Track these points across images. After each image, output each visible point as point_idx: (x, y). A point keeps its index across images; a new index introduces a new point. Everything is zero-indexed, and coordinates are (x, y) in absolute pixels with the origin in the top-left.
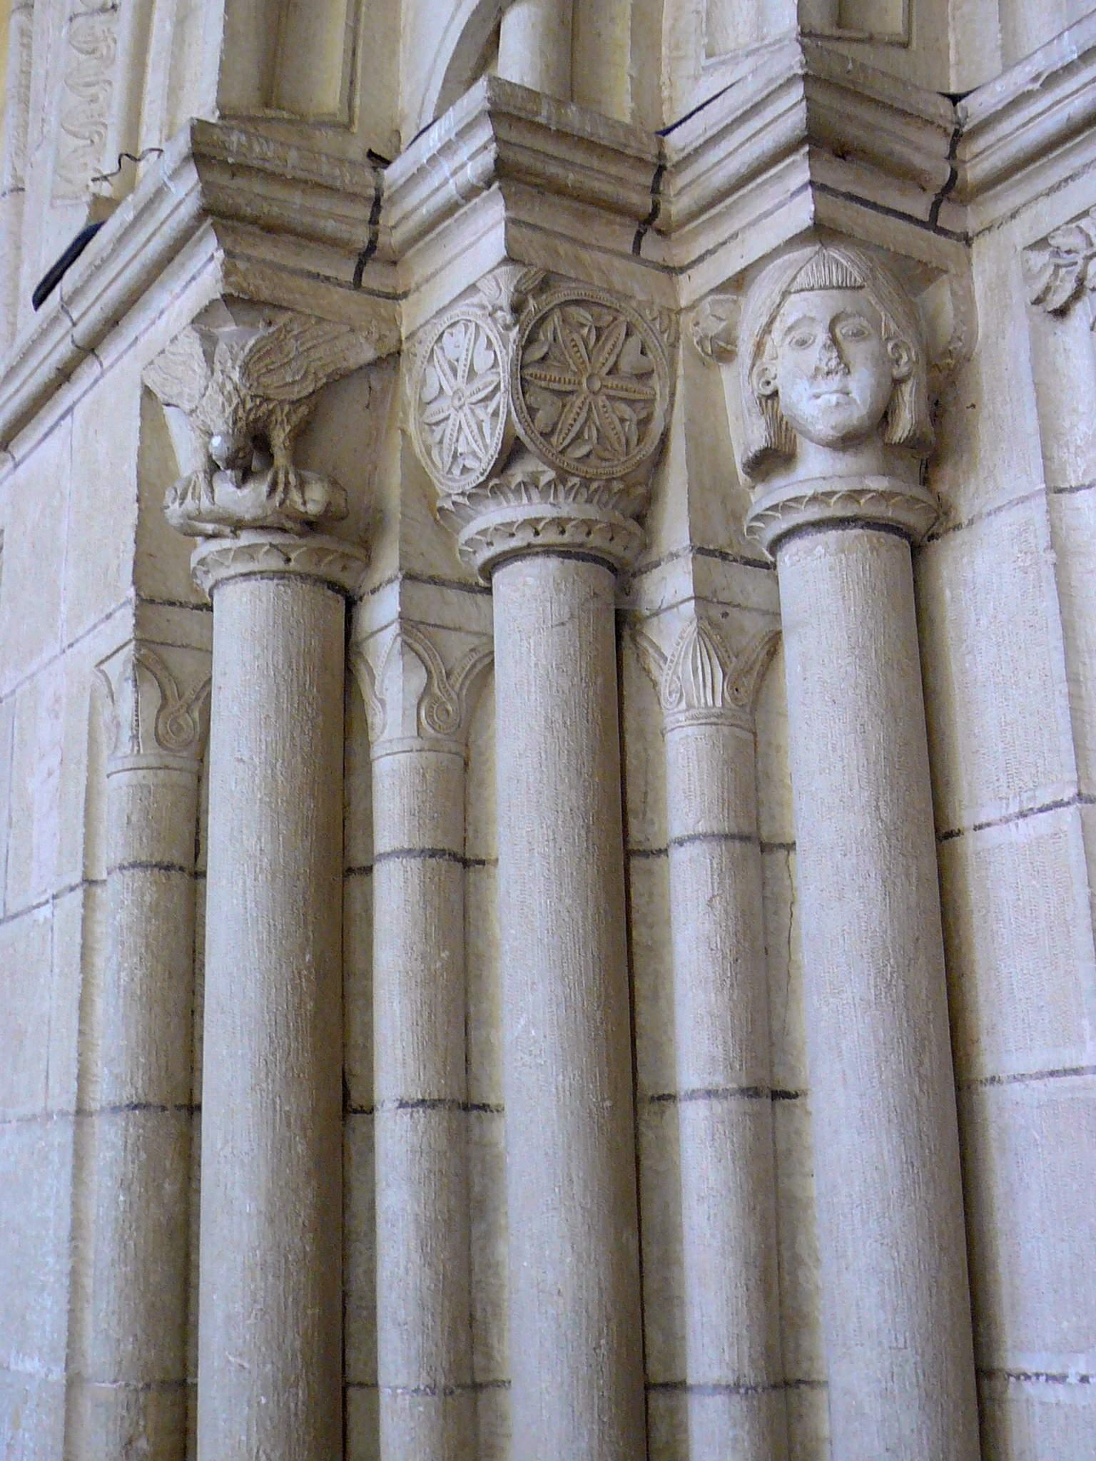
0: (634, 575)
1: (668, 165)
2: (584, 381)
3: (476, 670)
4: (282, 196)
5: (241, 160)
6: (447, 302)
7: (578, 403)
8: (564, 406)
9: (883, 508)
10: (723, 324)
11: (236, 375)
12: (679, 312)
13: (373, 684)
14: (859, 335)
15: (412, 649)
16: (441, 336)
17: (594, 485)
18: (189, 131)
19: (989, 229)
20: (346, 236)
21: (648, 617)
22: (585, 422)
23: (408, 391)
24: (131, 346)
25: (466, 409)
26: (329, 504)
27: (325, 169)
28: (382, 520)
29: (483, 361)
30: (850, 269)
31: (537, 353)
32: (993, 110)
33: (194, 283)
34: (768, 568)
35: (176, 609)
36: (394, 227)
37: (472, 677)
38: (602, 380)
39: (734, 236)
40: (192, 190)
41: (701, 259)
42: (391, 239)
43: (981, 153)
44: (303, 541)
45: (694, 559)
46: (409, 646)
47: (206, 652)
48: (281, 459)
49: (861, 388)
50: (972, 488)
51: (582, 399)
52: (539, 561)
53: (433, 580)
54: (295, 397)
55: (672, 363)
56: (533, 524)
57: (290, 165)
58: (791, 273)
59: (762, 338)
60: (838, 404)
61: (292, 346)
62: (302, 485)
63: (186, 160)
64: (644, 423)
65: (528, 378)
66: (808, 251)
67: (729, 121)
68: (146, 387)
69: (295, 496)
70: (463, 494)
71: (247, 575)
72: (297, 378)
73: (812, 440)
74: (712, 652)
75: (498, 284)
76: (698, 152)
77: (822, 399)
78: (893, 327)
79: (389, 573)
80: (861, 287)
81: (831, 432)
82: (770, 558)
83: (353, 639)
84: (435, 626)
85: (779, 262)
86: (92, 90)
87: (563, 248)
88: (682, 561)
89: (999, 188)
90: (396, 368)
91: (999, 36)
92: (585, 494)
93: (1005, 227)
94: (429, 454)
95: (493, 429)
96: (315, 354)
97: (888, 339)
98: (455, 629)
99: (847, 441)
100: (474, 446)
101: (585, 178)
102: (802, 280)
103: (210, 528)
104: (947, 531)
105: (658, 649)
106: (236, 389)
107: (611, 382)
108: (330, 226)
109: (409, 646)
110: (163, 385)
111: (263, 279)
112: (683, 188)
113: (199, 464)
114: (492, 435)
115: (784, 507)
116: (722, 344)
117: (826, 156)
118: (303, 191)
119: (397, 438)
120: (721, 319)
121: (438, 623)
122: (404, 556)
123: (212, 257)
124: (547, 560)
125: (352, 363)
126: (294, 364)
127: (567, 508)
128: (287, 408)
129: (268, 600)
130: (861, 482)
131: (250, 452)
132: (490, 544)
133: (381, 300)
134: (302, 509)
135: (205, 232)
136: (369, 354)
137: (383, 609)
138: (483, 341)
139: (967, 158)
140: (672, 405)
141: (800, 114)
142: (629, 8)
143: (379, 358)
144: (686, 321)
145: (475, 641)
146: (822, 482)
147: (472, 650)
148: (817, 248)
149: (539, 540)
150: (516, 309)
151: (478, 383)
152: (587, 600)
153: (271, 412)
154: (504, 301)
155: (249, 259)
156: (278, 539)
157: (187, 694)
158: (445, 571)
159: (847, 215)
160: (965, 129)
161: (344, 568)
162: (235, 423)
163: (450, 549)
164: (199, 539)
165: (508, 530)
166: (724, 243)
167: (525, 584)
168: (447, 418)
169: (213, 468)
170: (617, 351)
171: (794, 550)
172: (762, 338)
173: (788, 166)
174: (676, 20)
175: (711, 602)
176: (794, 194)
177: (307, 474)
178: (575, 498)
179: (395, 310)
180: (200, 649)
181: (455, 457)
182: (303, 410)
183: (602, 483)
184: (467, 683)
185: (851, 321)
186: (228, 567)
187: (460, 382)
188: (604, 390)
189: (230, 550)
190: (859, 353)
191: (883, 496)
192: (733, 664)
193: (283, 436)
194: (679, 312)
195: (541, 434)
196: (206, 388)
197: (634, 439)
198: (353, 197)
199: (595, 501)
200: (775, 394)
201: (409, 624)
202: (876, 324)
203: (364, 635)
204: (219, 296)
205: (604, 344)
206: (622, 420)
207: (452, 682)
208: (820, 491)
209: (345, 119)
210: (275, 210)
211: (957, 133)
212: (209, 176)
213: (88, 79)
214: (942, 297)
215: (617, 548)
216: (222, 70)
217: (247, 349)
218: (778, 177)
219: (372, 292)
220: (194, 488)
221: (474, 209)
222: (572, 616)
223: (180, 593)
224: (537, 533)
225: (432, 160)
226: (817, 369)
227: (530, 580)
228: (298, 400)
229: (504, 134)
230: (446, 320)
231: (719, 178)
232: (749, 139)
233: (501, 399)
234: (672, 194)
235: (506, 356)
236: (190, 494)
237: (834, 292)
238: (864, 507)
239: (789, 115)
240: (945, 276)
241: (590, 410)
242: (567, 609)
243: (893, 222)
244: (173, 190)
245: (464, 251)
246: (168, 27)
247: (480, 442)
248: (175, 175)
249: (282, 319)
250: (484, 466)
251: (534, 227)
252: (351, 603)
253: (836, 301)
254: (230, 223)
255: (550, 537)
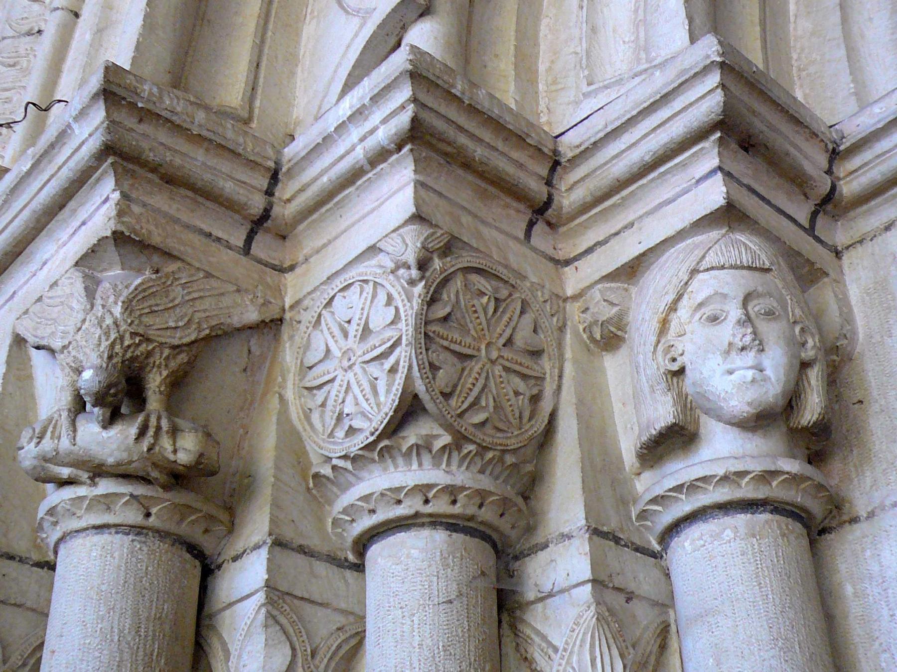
0: (516, 558)
1: (563, 160)
2: (483, 347)
3: (342, 652)
4: (180, 163)
5: (150, 106)
6: (341, 266)
7: (477, 368)
8: (463, 370)
9: (793, 493)
10: (615, 310)
11: (117, 310)
12: (565, 300)
13: (227, 659)
14: (770, 314)
15: (277, 622)
16: (332, 299)
17: (490, 455)
18: (102, 70)
19: (861, 242)
20: (243, 199)
21: (533, 603)
22: (483, 390)
23: (288, 358)
24: (7, 301)
25: (357, 368)
26: (201, 455)
27: (230, 134)
28: (249, 486)
29: (380, 317)
30: (758, 252)
31: (441, 311)
32: (873, 129)
33: (83, 228)
34: (656, 558)
35: (14, 564)
36: (289, 201)
37: (337, 659)
38: (499, 349)
39: (632, 224)
40: (97, 129)
41: (589, 251)
42: (284, 211)
43: (856, 171)
44: (167, 496)
45: (590, 539)
46: (274, 618)
47: (42, 614)
48: (154, 403)
49: (775, 363)
50: (869, 481)
51: (480, 365)
52: (426, 533)
53: (302, 550)
54: (176, 342)
55: (560, 345)
56: (423, 490)
57: (197, 123)
58: (699, 253)
59: (667, 315)
60: (753, 381)
61: (178, 293)
62: (174, 432)
63: (95, 97)
64: (535, 399)
65: (431, 334)
66: (715, 234)
67: (634, 113)
68: (18, 335)
69: (166, 443)
70: (345, 457)
71: (100, 528)
72: (181, 324)
73: (719, 419)
74: (611, 641)
75: (404, 241)
76: (597, 145)
77: (734, 374)
78: (798, 311)
79: (256, 539)
80: (768, 270)
81: (747, 408)
82: (657, 547)
83: (206, 610)
84: (302, 599)
85: (682, 245)
86: (7, 94)
87: (466, 219)
88: (576, 542)
89: (873, 203)
90: (277, 337)
91: (852, 85)
92: (479, 463)
93: (879, 239)
94: (308, 418)
95: (389, 386)
96: (199, 306)
97: (795, 322)
98: (321, 604)
99: (758, 421)
100: (365, 405)
101: (484, 162)
102: (711, 259)
103: (65, 472)
104: (842, 524)
105: (544, 638)
106: (116, 323)
107: (507, 353)
108: (228, 187)
109: (274, 618)
110: (36, 329)
111: (157, 228)
112: (576, 183)
113: (64, 403)
114: (388, 391)
115: (692, 487)
116: (613, 329)
117: (734, 146)
118: (207, 150)
119: (275, 403)
120: (612, 304)
121: (306, 596)
122: (273, 521)
123: (107, 199)
124: (434, 532)
125: (236, 321)
126: (178, 310)
127: (461, 476)
128: (167, 352)
129: (121, 557)
130: (774, 463)
131: (122, 394)
132: (373, 511)
133: (268, 270)
134: (172, 457)
135: (105, 172)
136: (252, 316)
137: (247, 577)
138: (382, 297)
139: (842, 175)
140: (559, 387)
141: (718, 97)
142: (512, 48)
143: (263, 321)
144: (573, 309)
145: (341, 620)
146: (732, 461)
147: (339, 629)
148: (724, 231)
149: (428, 509)
150: (423, 265)
151: (373, 341)
152: (474, 578)
153: (149, 354)
154: (411, 257)
155: (144, 205)
156: (140, 490)
157: (13, 659)
158: (314, 542)
159: (749, 203)
160: (842, 148)
161: (206, 531)
162: (110, 358)
163: (321, 520)
164: (50, 487)
165: (395, 495)
166: (617, 234)
167: (408, 556)
168: (332, 381)
169: (79, 406)
170: (513, 324)
171: (697, 535)
172: (667, 315)
173: (693, 155)
174: (552, 62)
175: (608, 587)
176: (699, 181)
177: (180, 422)
178: (467, 468)
179: (280, 281)
180: (33, 610)
181: (339, 418)
182: (183, 358)
183: (497, 453)
184: (333, 664)
185: (761, 301)
186: (80, 517)
187: (351, 342)
188: (501, 361)
189: (85, 497)
190: (771, 331)
191: (795, 479)
192: (631, 655)
193: (158, 379)
194: (565, 300)
195: (441, 393)
196: (84, 321)
197: (526, 415)
198: (253, 165)
199: (488, 472)
200: (682, 371)
201: (276, 595)
202: (784, 307)
203: (221, 606)
204: (109, 234)
205: (501, 317)
206: (517, 393)
207: (317, 662)
208: (733, 469)
209: (246, 115)
210: (178, 161)
211: (830, 197)
212: (116, 116)
213: (5, 86)
214: (825, 295)
215: (504, 525)
216: (137, 48)
217: (132, 288)
218: (684, 165)
219: (260, 261)
220: (55, 428)
221: (379, 175)
222: (460, 594)
223: (21, 547)
224: (427, 501)
225: (341, 127)
226: (730, 344)
227: (415, 553)
228: (178, 346)
229: (422, 97)
230: (339, 283)
231: (620, 169)
232: (655, 129)
233: (403, 354)
234: (563, 189)
235: (409, 308)
236: (49, 434)
237: (744, 272)
238: (775, 490)
239: (705, 101)
240: (826, 280)
241: (487, 378)
242: (455, 586)
243: (786, 222)
244: (77, 132)
245: (364, 217)
246: (88, 37)
247: (372, 400)
248: (82, 114)
249: (172, 267)
250: (374, 424)
251: (440, 194)
252: (208, 570)
253: (750, 280)
254: (130, 166)
255: (440, 506)
